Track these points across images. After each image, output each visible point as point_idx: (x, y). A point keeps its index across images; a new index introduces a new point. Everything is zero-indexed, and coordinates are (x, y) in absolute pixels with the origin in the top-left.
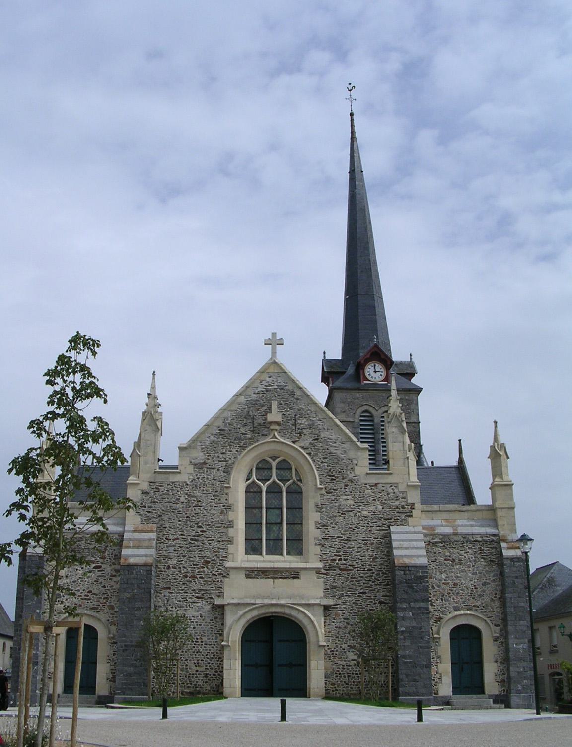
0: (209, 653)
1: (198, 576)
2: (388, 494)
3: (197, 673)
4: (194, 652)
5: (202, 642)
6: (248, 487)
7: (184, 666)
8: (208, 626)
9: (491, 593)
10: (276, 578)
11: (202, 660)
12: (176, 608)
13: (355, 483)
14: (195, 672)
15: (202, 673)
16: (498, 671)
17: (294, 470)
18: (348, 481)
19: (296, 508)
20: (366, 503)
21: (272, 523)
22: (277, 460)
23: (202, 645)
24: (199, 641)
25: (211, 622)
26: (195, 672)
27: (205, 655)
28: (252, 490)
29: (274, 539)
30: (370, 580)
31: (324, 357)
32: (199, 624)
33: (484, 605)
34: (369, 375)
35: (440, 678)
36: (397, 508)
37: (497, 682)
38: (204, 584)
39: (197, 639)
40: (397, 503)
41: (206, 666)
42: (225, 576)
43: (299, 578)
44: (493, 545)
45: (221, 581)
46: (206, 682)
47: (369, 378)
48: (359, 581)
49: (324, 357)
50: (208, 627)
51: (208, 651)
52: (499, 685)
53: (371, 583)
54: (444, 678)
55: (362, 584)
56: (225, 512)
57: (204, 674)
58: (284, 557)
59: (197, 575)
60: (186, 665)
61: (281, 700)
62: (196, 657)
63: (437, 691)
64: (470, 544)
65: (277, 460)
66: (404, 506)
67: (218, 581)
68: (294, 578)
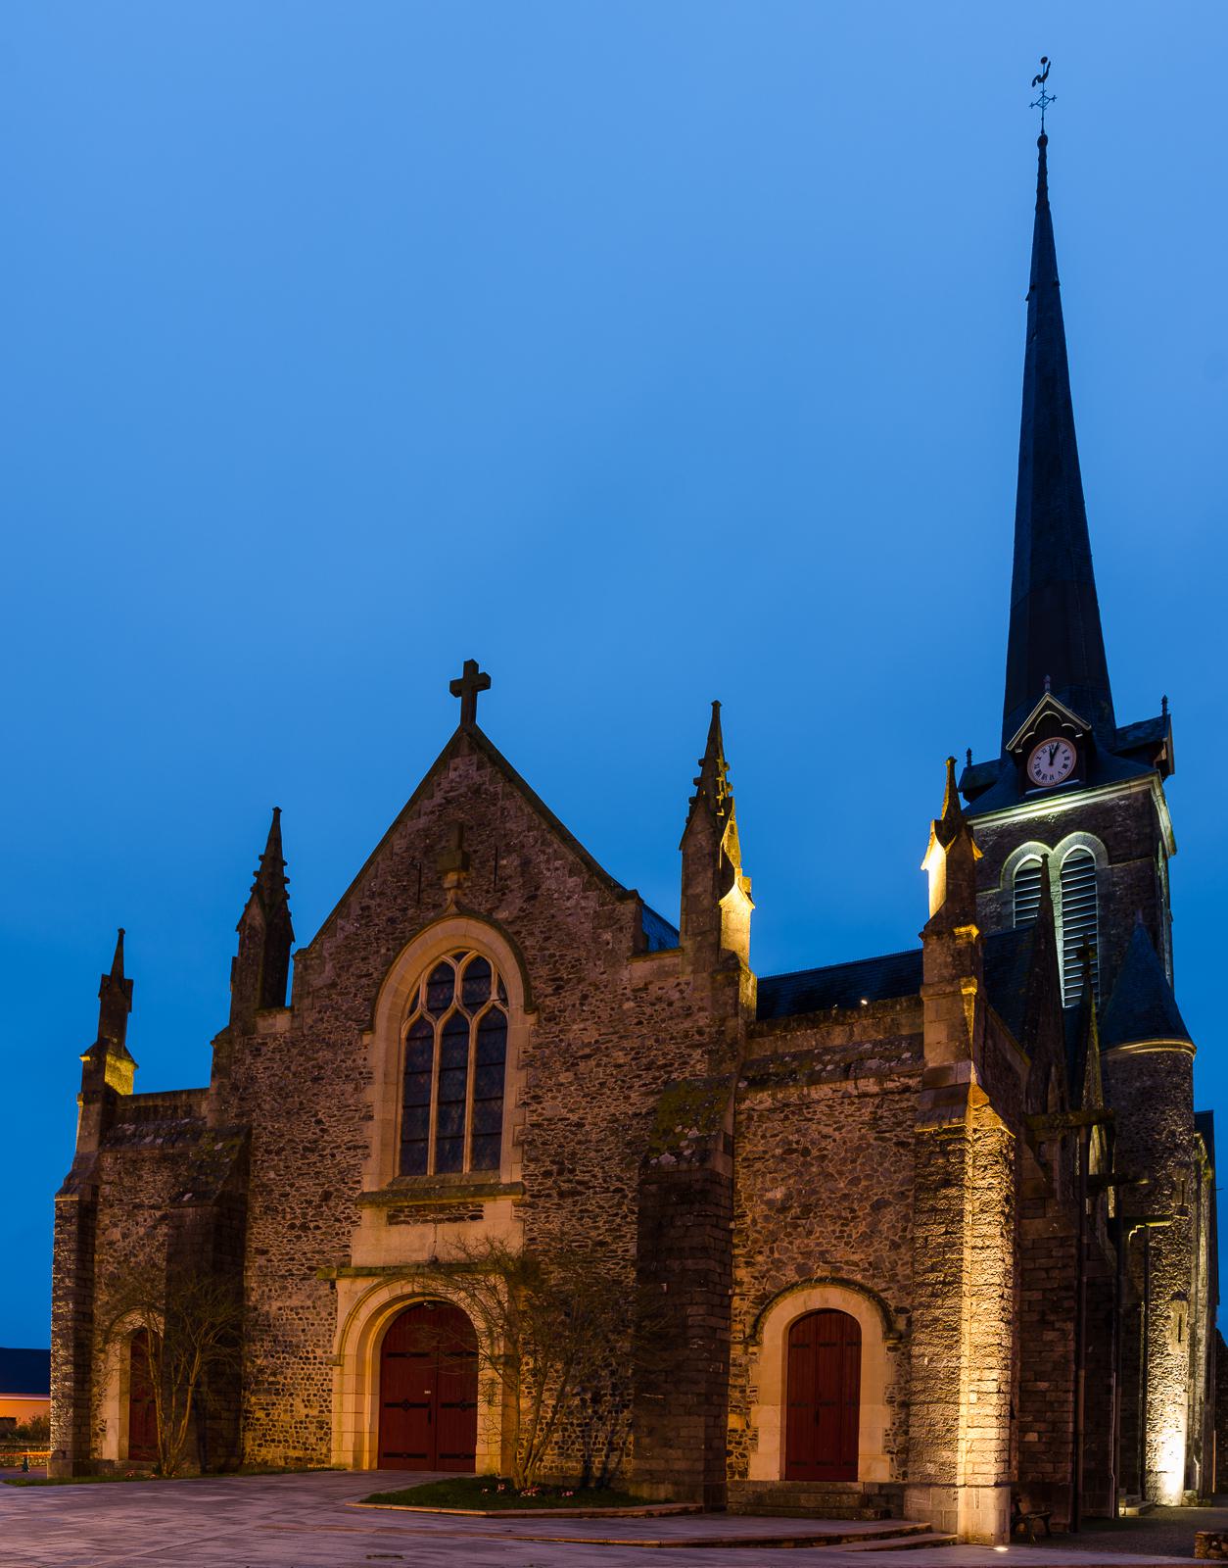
0: (325, 1380)
1: (312, 1225)
2: (670, 1004)
3: (308, 1420)
4: (302, 1379)
5: (315, 1358)
6: (413, 1029)
7: (288, 1407)
8: (324, 1325)
9: (893, 1226)
10: (441, 1221)
11: (315, 1395)
12: (276, 1291)
13: (603, 989)
14: (304, 1419)
15: (315, 1421)
16: (894, 1424)
17: (494, 979)
18: (590, 984)
19: (492, 1065)
20: (624, 1034)
21: (451, 1102)
22: (465, 961)
23: (314, 1364)
24: (311, 1356)
25: (329, 1318)
26: (304, 1419)
27: (319, 1383)
28: (418, 1035)
29: (452, 1138)
30: (616, 1215)
31: (969, 762)
32: (310, 1322)
33: (871, 1259)
34: (1039, 773)
35: (755, 1438)
36: (686, 1036)
37: (889, 1452)
38: (322, 1240)
39: (308, 1352)
40: (687, 1024)
41: (321, 1406)
42: (355, 1222)
43: (481, 1217)
44: (908, 1100)
45: (349, 1232)
46: (321, 1439)
47: (1038, 779)
48: (598, 1216)
49: (969, 762)
50: (324, 1329)
51: (325, 1377)
52: (892, 1459)
53: (618, 1220)
54: (762, 1437)
55: (601, 1224)
56: (363, 1086)
57: (318, 1422)
58: (56, 1196)
59: (311, 1221)
60: (292, 1405)
61: (474, 1471)
62: (305, 1389)
63: (746, 1469)
64: (849, 1104)
65: (465, 961)
66: (702, 1027)
67: (343, 1234)
68: (474, 1218)
